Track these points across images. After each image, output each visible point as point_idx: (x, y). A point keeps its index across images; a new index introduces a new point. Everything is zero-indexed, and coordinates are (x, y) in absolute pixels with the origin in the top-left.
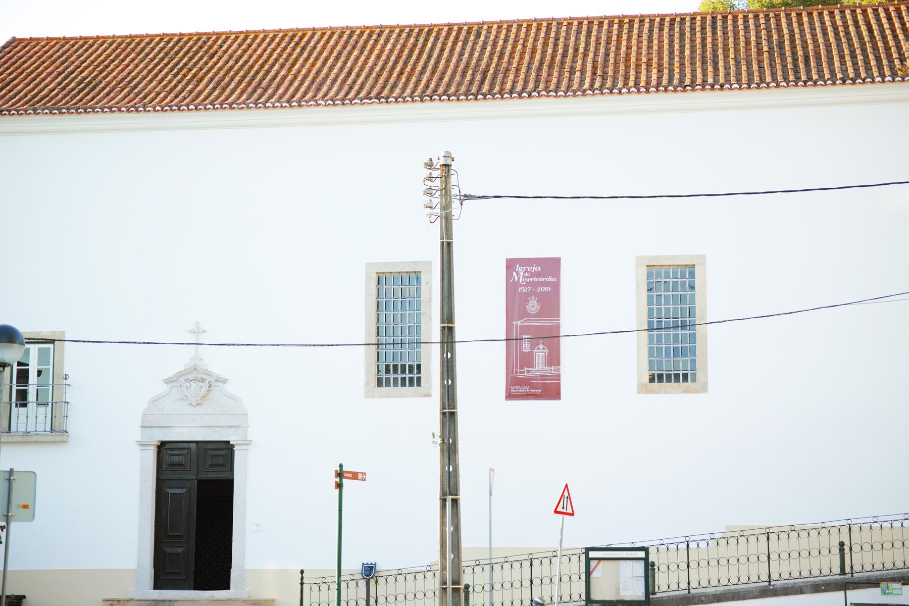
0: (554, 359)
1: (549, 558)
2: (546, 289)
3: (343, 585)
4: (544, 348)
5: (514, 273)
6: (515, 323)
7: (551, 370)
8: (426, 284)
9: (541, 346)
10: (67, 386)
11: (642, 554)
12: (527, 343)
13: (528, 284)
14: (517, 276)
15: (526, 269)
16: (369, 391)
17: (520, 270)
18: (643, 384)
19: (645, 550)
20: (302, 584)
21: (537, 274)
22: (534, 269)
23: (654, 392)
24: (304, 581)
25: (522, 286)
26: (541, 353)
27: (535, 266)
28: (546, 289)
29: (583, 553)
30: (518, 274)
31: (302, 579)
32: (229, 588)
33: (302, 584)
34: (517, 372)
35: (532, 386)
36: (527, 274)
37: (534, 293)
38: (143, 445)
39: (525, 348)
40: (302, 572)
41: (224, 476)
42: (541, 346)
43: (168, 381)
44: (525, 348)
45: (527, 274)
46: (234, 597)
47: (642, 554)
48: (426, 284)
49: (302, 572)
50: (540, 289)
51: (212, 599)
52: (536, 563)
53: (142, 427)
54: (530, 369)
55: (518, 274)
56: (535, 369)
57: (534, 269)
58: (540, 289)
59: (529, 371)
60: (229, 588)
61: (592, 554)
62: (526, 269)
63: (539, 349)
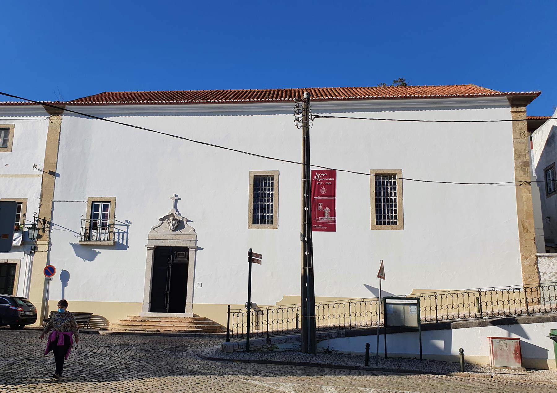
0: (333, 213)
1: (277, 309)
2: (329, 183)
3: (231, 314)
4: (328, 209)
5: (315, 176)
6: (315, 198)
7: (331, 218)
8: (276, 180)
9: (327, 208)
10: (115, 219)
11: (415, 302)
12: (320, 205)
13: (321, 181)
14: (316, 177)
15: (321, 175)
16: (250, 226)
17: (318, 175)
18: (373, 225)
19: (418, 299)
20: (229, 313)
21: (325, 177)
22: (324, 174)
23: (376, 229)
24: (230, 311)
25: (319, 182)
26: (327, 211)
27: (325, 173)
28: (329, 183)
29: (345, 325)
30: (317, 177)
31: (229, 309)
32: (184, 312)
33: (229, 313)
34: (316, 219)
35: (323, 225)
36: (320, 177)
37: (324, 185)
38: (149, 248)
39: (320, 209)
40: (229, 306)
41: (186, 262)
42: (327, 208)
43: (161, 220)
44: (320, 209)
45: (320, 177)
46: (186, 316)
47: (415, 302)
48: (276, 180)
49: (229, 306)
50: (326, 183)
51: (177, 317)
52: (270, 312)
53: (148, 239)
54: (322, 218)
55: (317, 177)
56: (324, 218)
57: (324, 174)
58: (326, 183)
59: (321, 219)
60: (184, 312)
61: (125, 234)
62: (321, 175)
63: (326, 209)
